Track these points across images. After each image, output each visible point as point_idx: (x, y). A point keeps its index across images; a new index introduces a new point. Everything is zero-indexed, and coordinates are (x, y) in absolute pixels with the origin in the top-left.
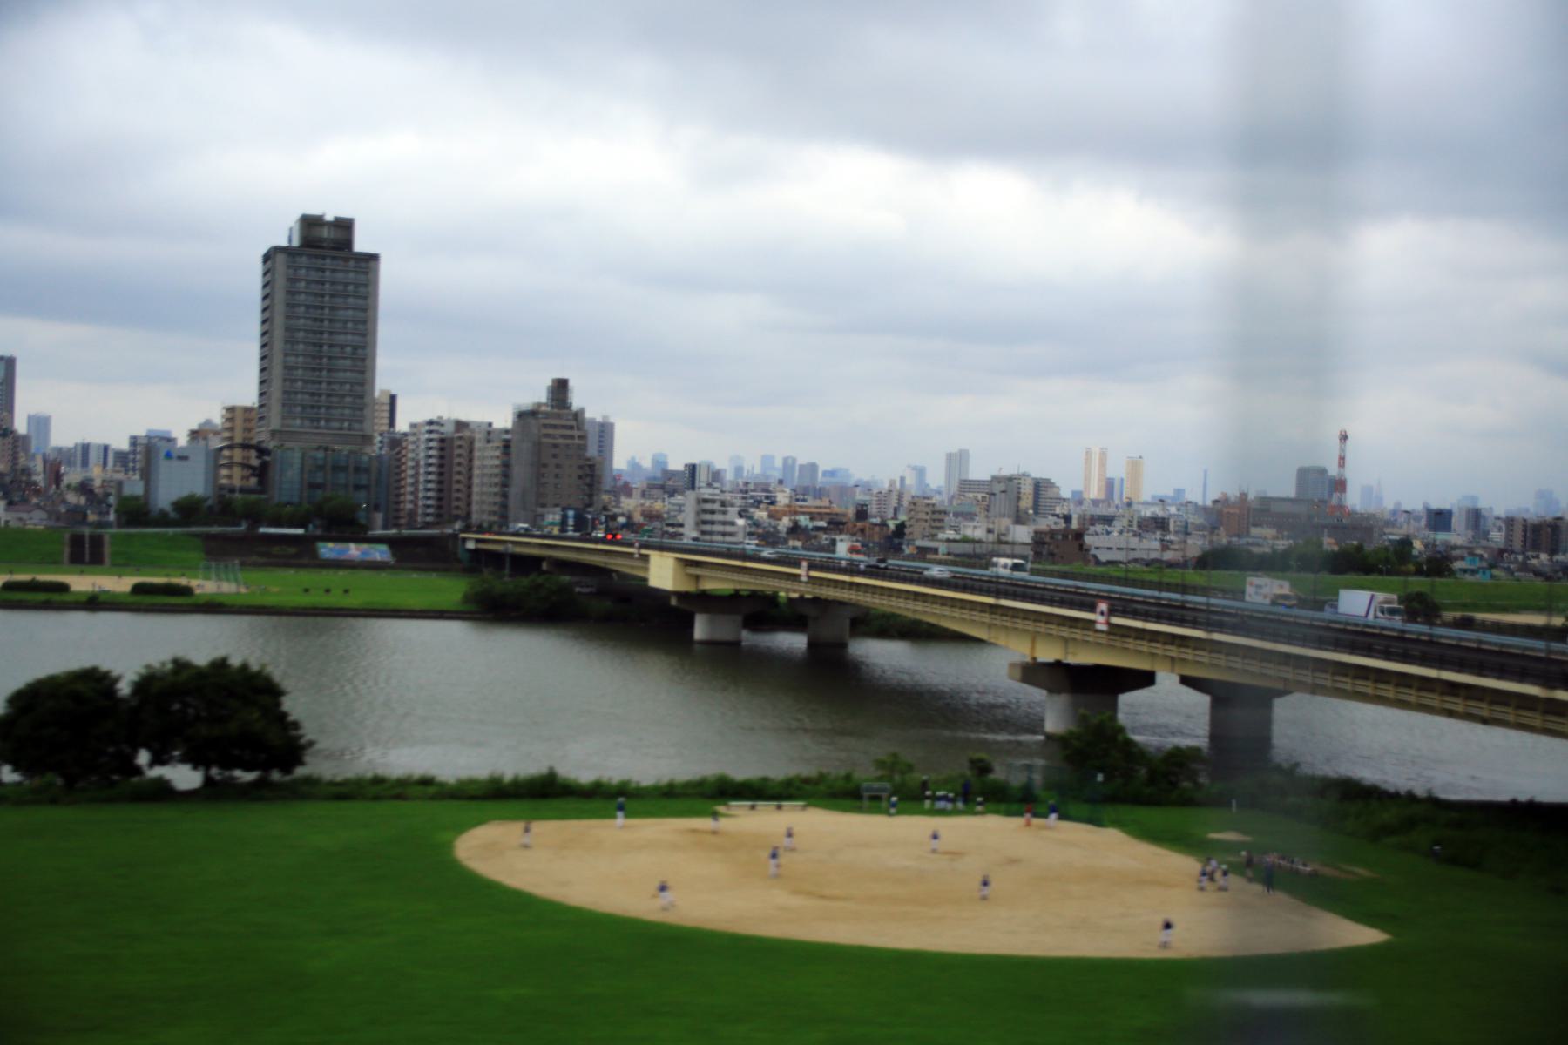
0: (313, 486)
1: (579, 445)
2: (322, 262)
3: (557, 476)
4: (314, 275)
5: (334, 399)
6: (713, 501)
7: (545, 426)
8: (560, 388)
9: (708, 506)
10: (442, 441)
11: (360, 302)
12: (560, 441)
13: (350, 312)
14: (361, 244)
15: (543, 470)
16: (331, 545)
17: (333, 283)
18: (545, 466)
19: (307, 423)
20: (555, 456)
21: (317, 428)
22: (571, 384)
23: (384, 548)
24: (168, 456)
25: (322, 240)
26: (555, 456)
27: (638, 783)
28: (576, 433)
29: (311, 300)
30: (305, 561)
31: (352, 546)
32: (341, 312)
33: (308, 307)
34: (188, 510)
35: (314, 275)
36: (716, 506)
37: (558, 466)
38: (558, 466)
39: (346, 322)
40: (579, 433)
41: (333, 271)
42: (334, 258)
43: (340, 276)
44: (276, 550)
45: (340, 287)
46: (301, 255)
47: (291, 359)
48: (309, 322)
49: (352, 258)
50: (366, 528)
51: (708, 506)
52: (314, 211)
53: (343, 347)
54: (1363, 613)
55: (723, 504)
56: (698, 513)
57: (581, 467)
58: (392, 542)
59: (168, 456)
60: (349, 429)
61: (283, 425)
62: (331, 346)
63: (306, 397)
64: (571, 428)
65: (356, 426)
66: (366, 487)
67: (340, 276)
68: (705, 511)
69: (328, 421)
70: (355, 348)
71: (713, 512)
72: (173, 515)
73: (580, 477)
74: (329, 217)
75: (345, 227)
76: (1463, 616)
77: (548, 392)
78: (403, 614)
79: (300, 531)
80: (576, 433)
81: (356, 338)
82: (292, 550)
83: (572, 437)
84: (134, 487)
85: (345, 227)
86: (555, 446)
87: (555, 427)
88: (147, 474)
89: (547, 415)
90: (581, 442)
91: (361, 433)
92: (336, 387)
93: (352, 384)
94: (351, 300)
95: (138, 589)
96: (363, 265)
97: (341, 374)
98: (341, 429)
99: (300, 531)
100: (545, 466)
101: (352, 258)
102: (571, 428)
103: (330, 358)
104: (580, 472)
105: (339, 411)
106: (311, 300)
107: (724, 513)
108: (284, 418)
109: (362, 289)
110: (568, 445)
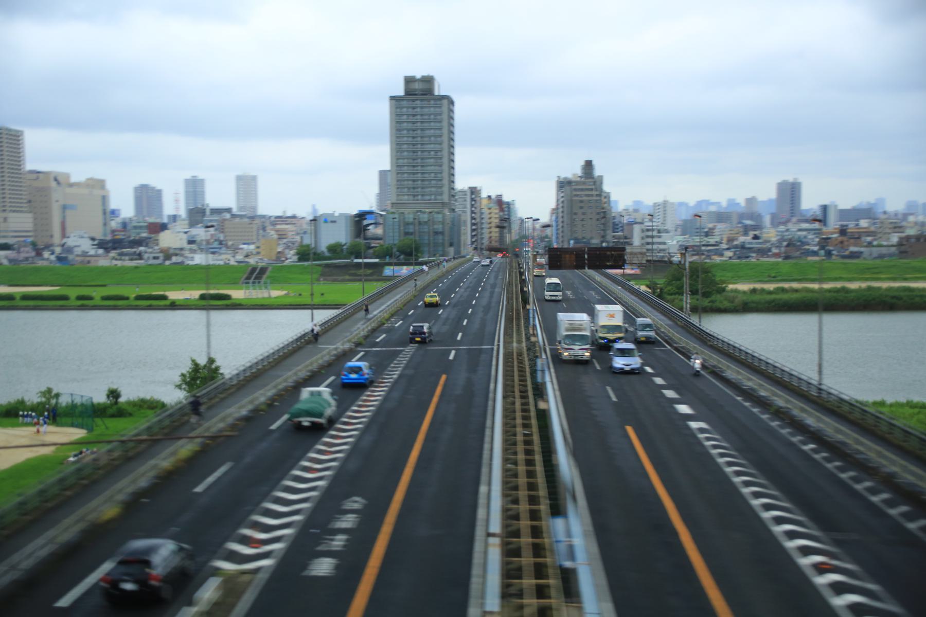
0: (407, 234)
1: (597, 200)
2: (428, 103)
3: (582, 220)
4: (411, 111)
5: (426, 183)
6: (652, 230)
7: (575, 190)
8: (589, 165)
9: (650, 233)
11: (438, 124)
12: (585, 198)
13: (432, 131)
15: (575, 217)
17: (422, 115)
18: (576, 214)
19: (411, 198)
20: (581, 208)
21: (417, 200)
22: (594, 163)
24: (326, 221)
25: (415, 90)
26: (581, 208)
27: (171, 404)
28: (594, 193)
29: (410, 126)
30: (375, 277)
31: (405, 267)
32: (427, 132)
33: (408, 130)
34: (335, 250)
35: (411, 111)
36: (655, 233)
37: (584, 214)
38: (584, 214)
39: (430, 137)
40: (598, 193)
41: (422, 108)
42: (422, 100)
43: (426, 111)
44: (361, 271)
45: (426, 117)
46: (403, 100)
47: (401, 161)
48: (410, 139)
49: (432, 99)
50: (417, 257)
51: (650, 233)
52: (410, 74)
53: (429, 151)
54: (364, 284)
55: (659, 231)
56: (643, 238)
57: (598, 214)
58: (640, 266)
59: (326, 221)
60: (436, 200)
61: (397, 200)
62: (422, 152)
63: (410, 182)
64: (592, 190)
65: (439, 197)
66: (442, 233)
67: (426, 111)
68: (648, 237)
69: (423, 195)
70: (436, 152)
71: (652, 237)
72: (327, 254)
73: (598, 220)
74: (418, 76)
76: (870, 289)
77: (583, 169)
78: (179, 307)
79: (377, 260)
80: (594, 193)
81: (437, 146)
82: (369, 272)
83: (592, 195)
84: (307, 240)
85: (428, 81)
86: (582, 202)
87: (582, 190)
88: (316, 233)
89: (577, 183)
90: (598, 198)
91: (441, 202)
92: (426, 175)
93: (436, 173)
94: (432, 124)
95: (202, 297)
96: (438, 102)
97: (429, 168)
98: (430, 200)
99: (377, 260)
100: (576, 214)
101: (432, 99)
102: (592, 190)
103: (422, 159)
104: (598, 217)
105: (429, 189)
106: (410, 126)
107: (660, 237)
108: (398, 195)
109: (439, 117)
110: (590, 201)
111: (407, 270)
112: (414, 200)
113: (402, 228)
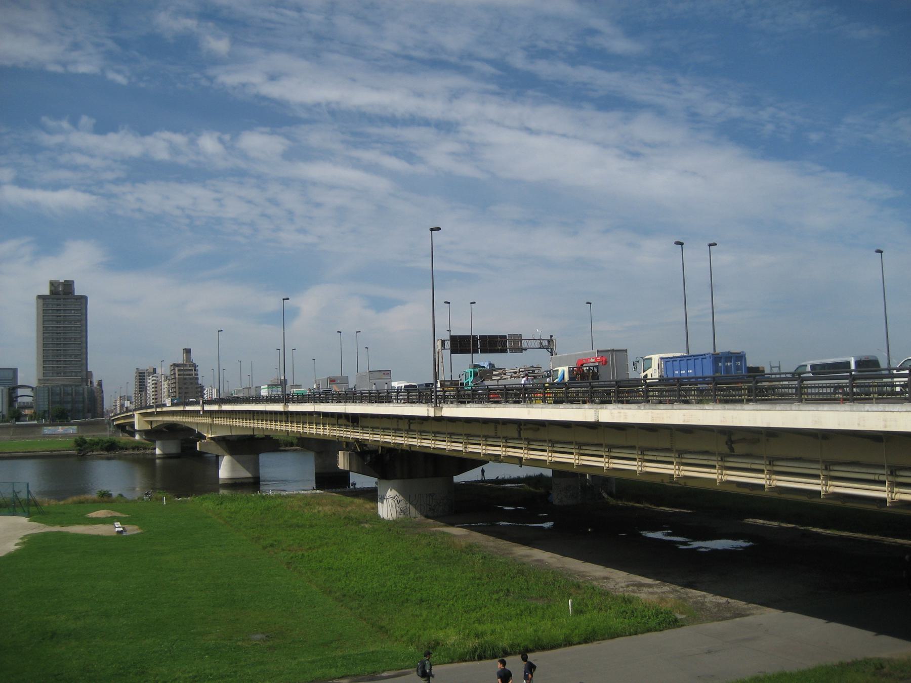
10: (156, 384)
14: (77, 292)
16: (50, 428)
19: (55, 375)
23: (75, 427)
31: (60, 427)
46: (49, 299)
64: (191, 370)
75: (69, 285)
85: (69, 285)
102: (191, 370)
111: (62, 429)
112: (57, 377)
113: (50, 398)
